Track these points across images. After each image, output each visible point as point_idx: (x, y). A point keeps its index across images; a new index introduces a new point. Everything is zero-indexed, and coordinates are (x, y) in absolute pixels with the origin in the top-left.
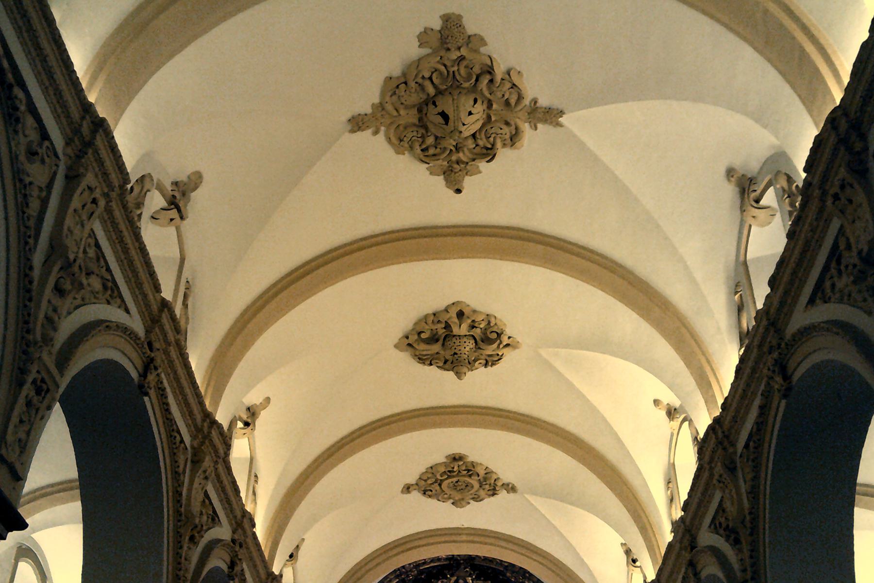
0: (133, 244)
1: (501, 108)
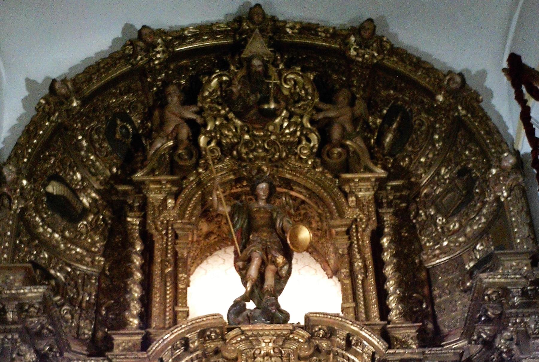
0: (39, 148)
1: (362, 314)
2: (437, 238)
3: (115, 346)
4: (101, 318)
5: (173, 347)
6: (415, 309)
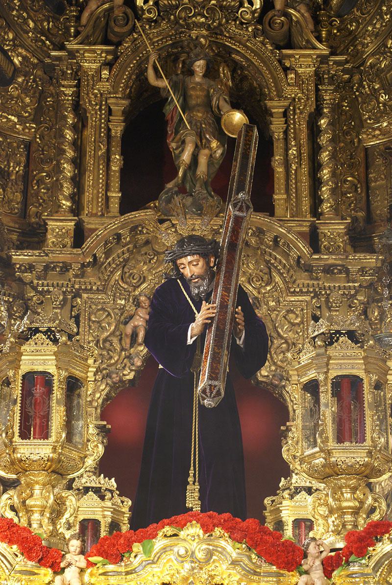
2: (368, 133)
3: (49, 231)
4: (32, 192)
5: (106, 242)
6: (349, 195)
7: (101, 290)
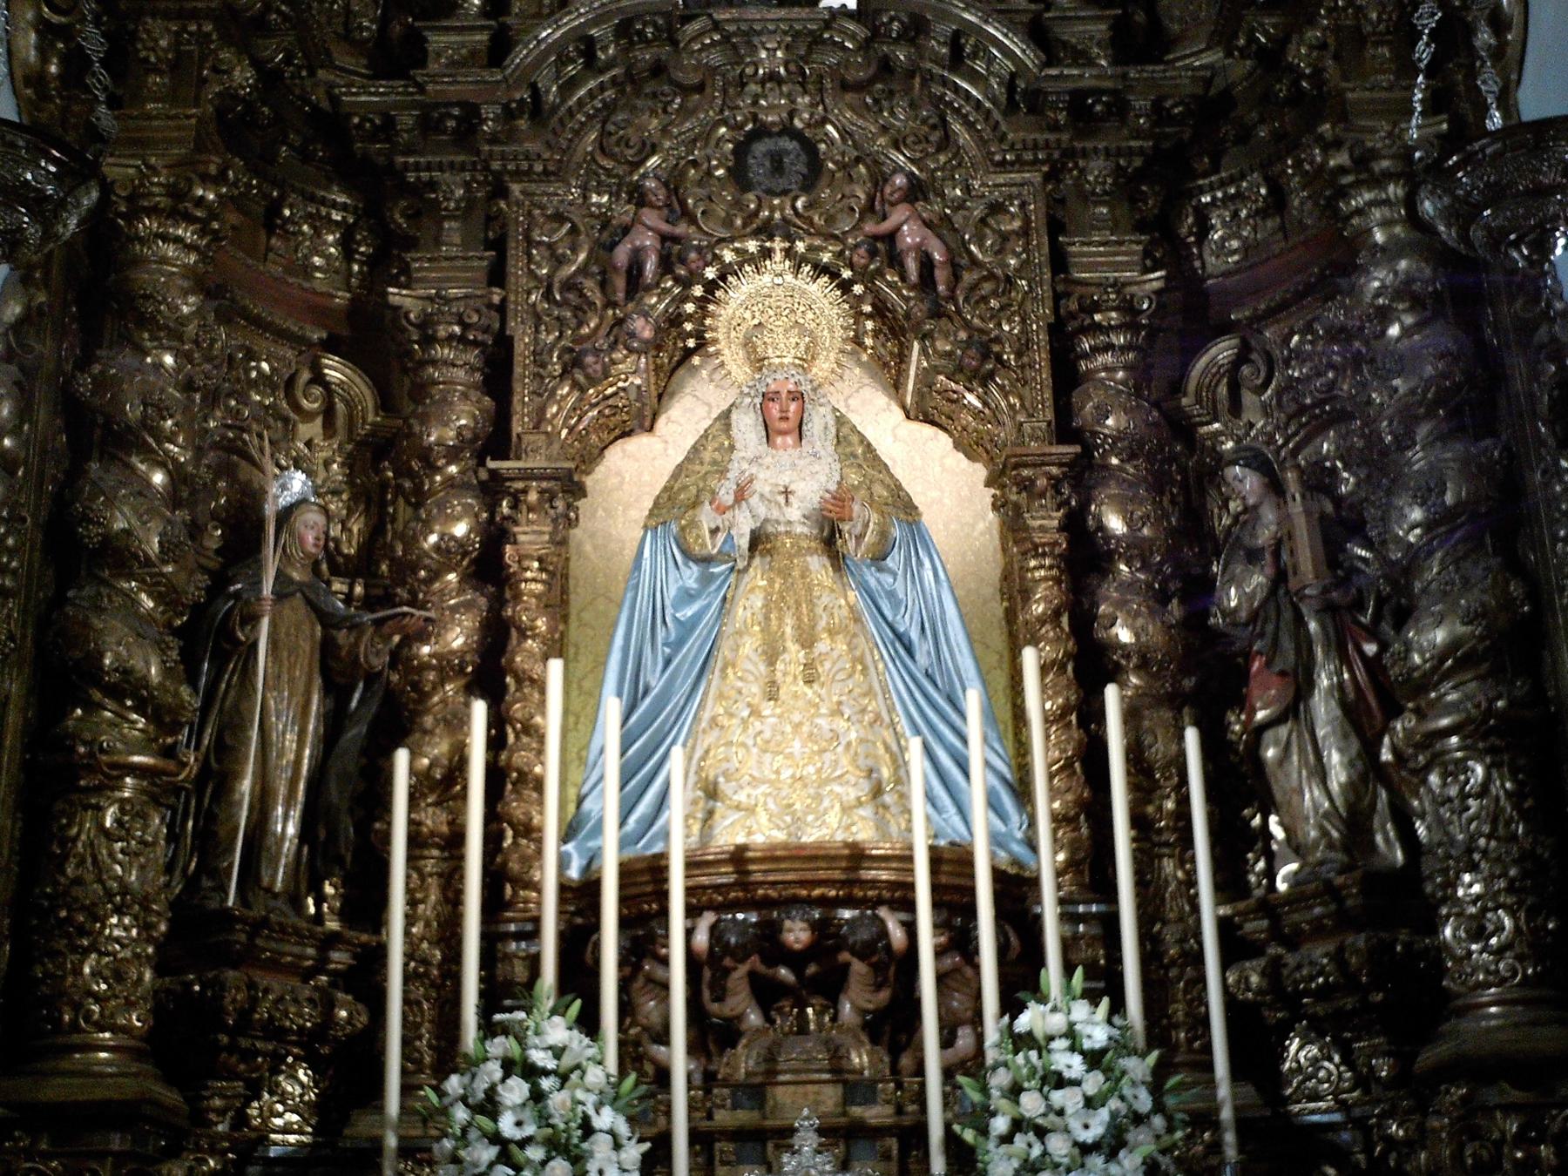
3: (432, 56)
7: (553, 173)
